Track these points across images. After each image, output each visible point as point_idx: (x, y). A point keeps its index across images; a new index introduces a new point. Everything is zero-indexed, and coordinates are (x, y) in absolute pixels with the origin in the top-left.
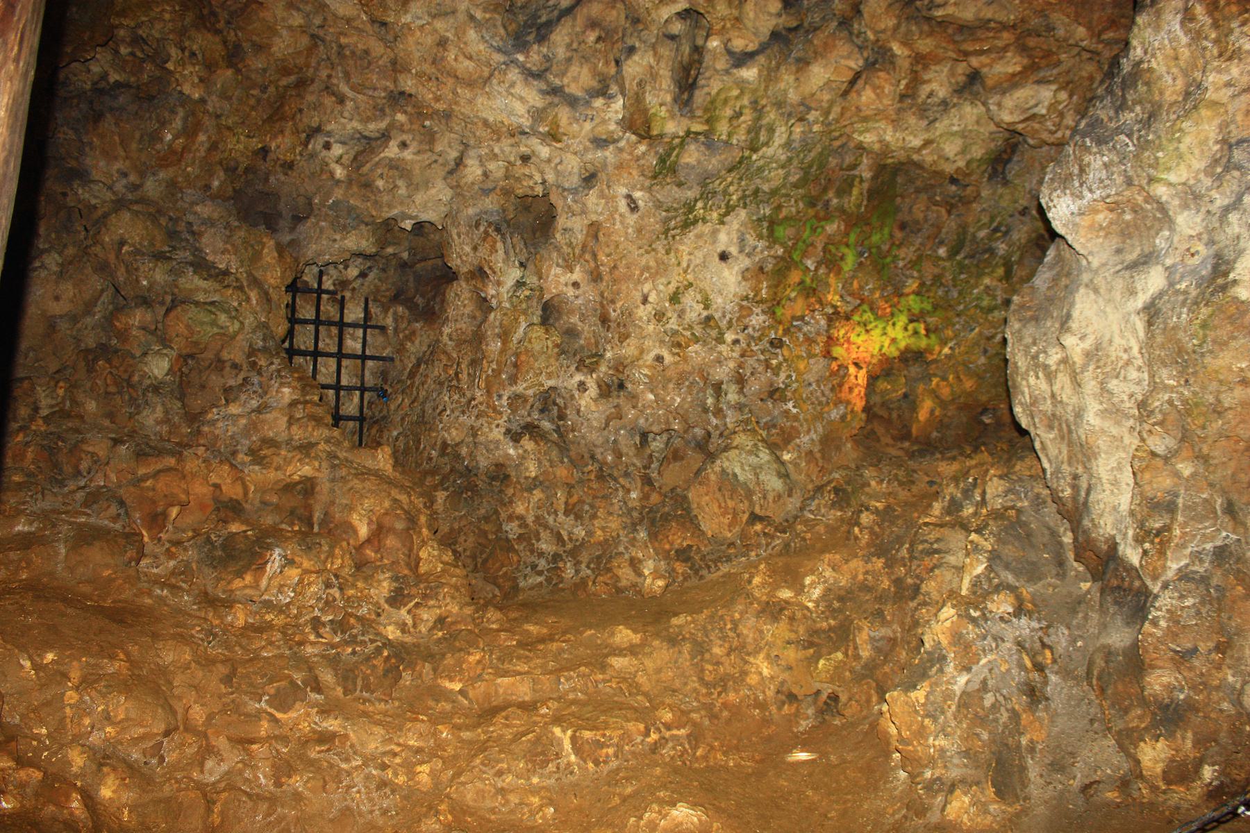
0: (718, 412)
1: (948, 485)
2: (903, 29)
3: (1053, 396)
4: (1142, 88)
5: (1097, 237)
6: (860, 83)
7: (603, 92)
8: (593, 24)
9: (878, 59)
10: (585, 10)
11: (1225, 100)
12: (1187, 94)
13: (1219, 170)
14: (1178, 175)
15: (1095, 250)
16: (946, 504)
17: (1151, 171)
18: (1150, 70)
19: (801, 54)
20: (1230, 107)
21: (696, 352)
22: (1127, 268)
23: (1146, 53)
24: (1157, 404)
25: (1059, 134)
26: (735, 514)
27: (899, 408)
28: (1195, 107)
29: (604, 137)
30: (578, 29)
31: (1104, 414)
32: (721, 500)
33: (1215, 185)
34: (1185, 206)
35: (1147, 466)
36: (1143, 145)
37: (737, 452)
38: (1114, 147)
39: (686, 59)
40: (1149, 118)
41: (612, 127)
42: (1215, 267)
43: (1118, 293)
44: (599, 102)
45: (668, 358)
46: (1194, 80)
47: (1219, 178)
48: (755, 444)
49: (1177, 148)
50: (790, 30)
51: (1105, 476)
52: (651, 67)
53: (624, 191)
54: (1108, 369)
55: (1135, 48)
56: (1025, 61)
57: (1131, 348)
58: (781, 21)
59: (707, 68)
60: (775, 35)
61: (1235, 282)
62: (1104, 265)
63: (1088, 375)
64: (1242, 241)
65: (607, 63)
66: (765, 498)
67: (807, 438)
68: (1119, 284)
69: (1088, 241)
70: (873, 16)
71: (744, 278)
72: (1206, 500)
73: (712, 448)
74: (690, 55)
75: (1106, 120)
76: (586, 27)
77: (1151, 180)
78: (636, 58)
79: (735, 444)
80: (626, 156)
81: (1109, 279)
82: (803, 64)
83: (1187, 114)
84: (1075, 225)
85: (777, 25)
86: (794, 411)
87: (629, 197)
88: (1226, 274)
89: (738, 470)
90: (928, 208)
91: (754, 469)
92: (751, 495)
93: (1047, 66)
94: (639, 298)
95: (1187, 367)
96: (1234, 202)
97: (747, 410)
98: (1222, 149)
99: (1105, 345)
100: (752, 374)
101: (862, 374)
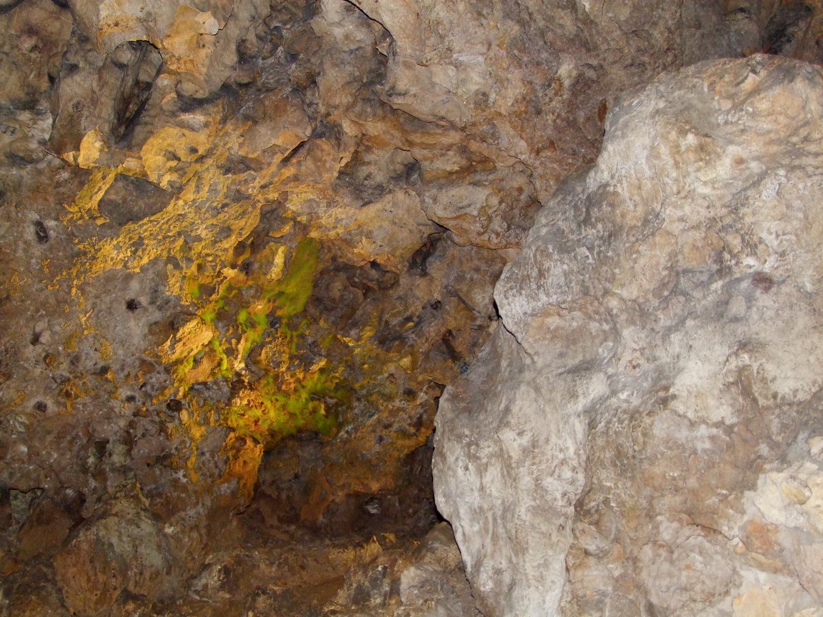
0: (100, 474)
1: (355, 573)
2: (357, 109)
3: (482, 489)
4: (605, 208)
5: (544, 339)
6: (303, 151)
7: (30, 105)
8: (31, 31)
9: (328, 130)
10: (24, 14)
11: (676, 232)
12: (646, 222)
13: (666, 293)
14: (630, 292)
15: (541, 351)
16: (352, 592)
17: (608, 285)
18: (615, 194)
19: (251, 112)
20: (679, 240)
21: (85, 405)
22: (569, 372)
23: (612, 177)
24: (593, 504)
25: (486, 237)
26: (105, 591)
27: (290, 489)
28: (653, 234)
29: (21, 154)
30: (13, 32)
31: (536, 511)
32: (91, 573)
33: (662, 306)
34: (632, 322)
35: (580, 565)
36: (602, 260)
37: (116, 519)
38: (575, 257)
39: (127, 90)
40: (610, 236)
41: (34, 145)
42: (656, 381)
43: (559, 395)
44: (25, 116)
45: (52, 407)
46: (653, 210)
47: (666, 300)
48: (138, 513)
49: (633, 268)
50: (241, 85)
51: (531, 572)
52: (93, 92)
53: (35, 216)
54: (543, 467)
55: (602, 172)
56: (464, 162)
57: (567, 448)
58: (234, 74)
59: (153, 106)
60: (226, 87)
61: (674, 397)
62: (548, 366)
63: (523, 470)
64: (682, 360)
65: (39, 75)
66: (141, 574)
67: (194, 511)
68: (561, 385)
69: (535, 341)
70: (329, 90)
71: (151, 332)
72: (632, 602)
73: (85, 514)
74: (132, 88)
75: (567, 231)
76: (23, 32)
77: (606, 292)
78: (77, 78)
79: (114, 512)
80: (44, 180)
81: (552, 380)
82: (252, 120)
83: (645, 238)
84: (526, 324)
85: (229, 77)
86: (184, 480)
87: (39, 225)
88: (666, 389)
89: (114, 540)
90: (345, 288)
91: (134, 540)
92: (127, 570)
93: (484, 170)
94: (29, 337)
95: (625, 471)
96: (677, 325)
97: (131, 474)
98: (670, 275)
99: (541, 443)
100: (143, 435)
101: (258, 451)
